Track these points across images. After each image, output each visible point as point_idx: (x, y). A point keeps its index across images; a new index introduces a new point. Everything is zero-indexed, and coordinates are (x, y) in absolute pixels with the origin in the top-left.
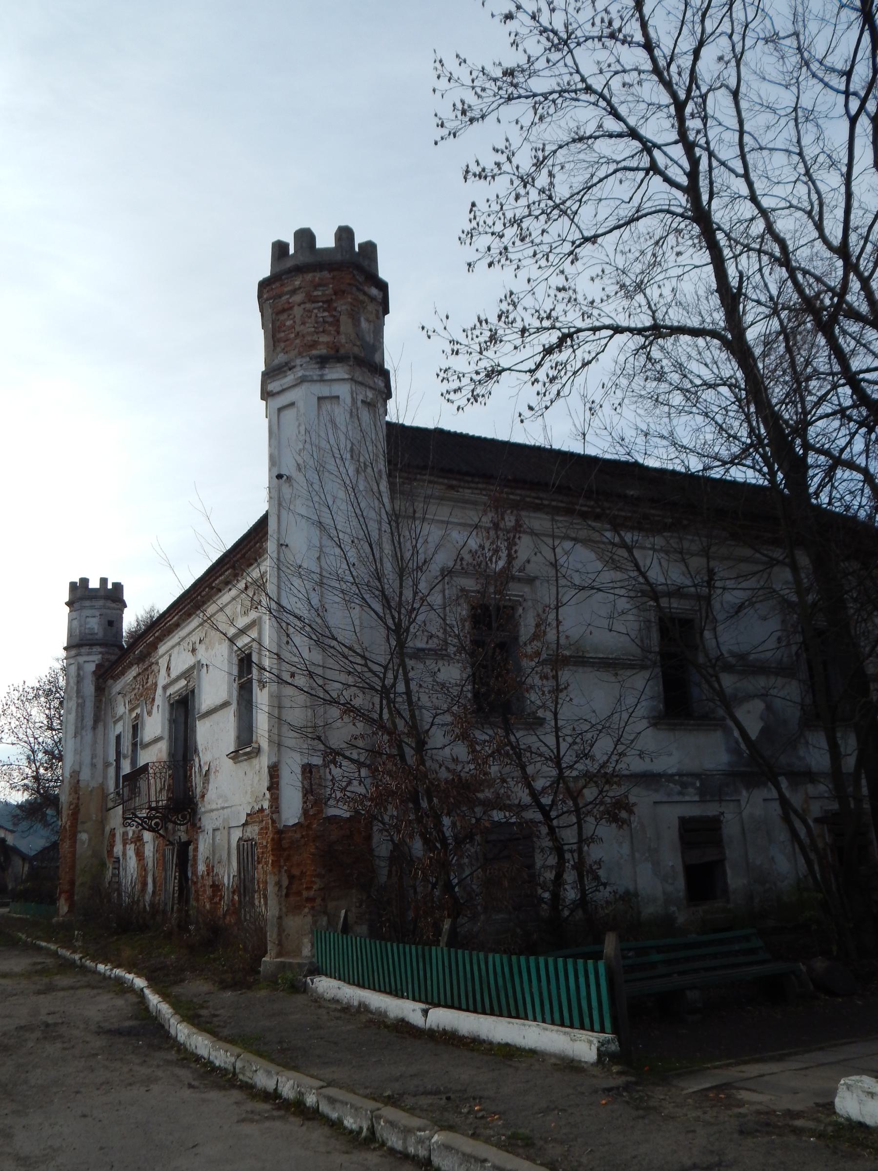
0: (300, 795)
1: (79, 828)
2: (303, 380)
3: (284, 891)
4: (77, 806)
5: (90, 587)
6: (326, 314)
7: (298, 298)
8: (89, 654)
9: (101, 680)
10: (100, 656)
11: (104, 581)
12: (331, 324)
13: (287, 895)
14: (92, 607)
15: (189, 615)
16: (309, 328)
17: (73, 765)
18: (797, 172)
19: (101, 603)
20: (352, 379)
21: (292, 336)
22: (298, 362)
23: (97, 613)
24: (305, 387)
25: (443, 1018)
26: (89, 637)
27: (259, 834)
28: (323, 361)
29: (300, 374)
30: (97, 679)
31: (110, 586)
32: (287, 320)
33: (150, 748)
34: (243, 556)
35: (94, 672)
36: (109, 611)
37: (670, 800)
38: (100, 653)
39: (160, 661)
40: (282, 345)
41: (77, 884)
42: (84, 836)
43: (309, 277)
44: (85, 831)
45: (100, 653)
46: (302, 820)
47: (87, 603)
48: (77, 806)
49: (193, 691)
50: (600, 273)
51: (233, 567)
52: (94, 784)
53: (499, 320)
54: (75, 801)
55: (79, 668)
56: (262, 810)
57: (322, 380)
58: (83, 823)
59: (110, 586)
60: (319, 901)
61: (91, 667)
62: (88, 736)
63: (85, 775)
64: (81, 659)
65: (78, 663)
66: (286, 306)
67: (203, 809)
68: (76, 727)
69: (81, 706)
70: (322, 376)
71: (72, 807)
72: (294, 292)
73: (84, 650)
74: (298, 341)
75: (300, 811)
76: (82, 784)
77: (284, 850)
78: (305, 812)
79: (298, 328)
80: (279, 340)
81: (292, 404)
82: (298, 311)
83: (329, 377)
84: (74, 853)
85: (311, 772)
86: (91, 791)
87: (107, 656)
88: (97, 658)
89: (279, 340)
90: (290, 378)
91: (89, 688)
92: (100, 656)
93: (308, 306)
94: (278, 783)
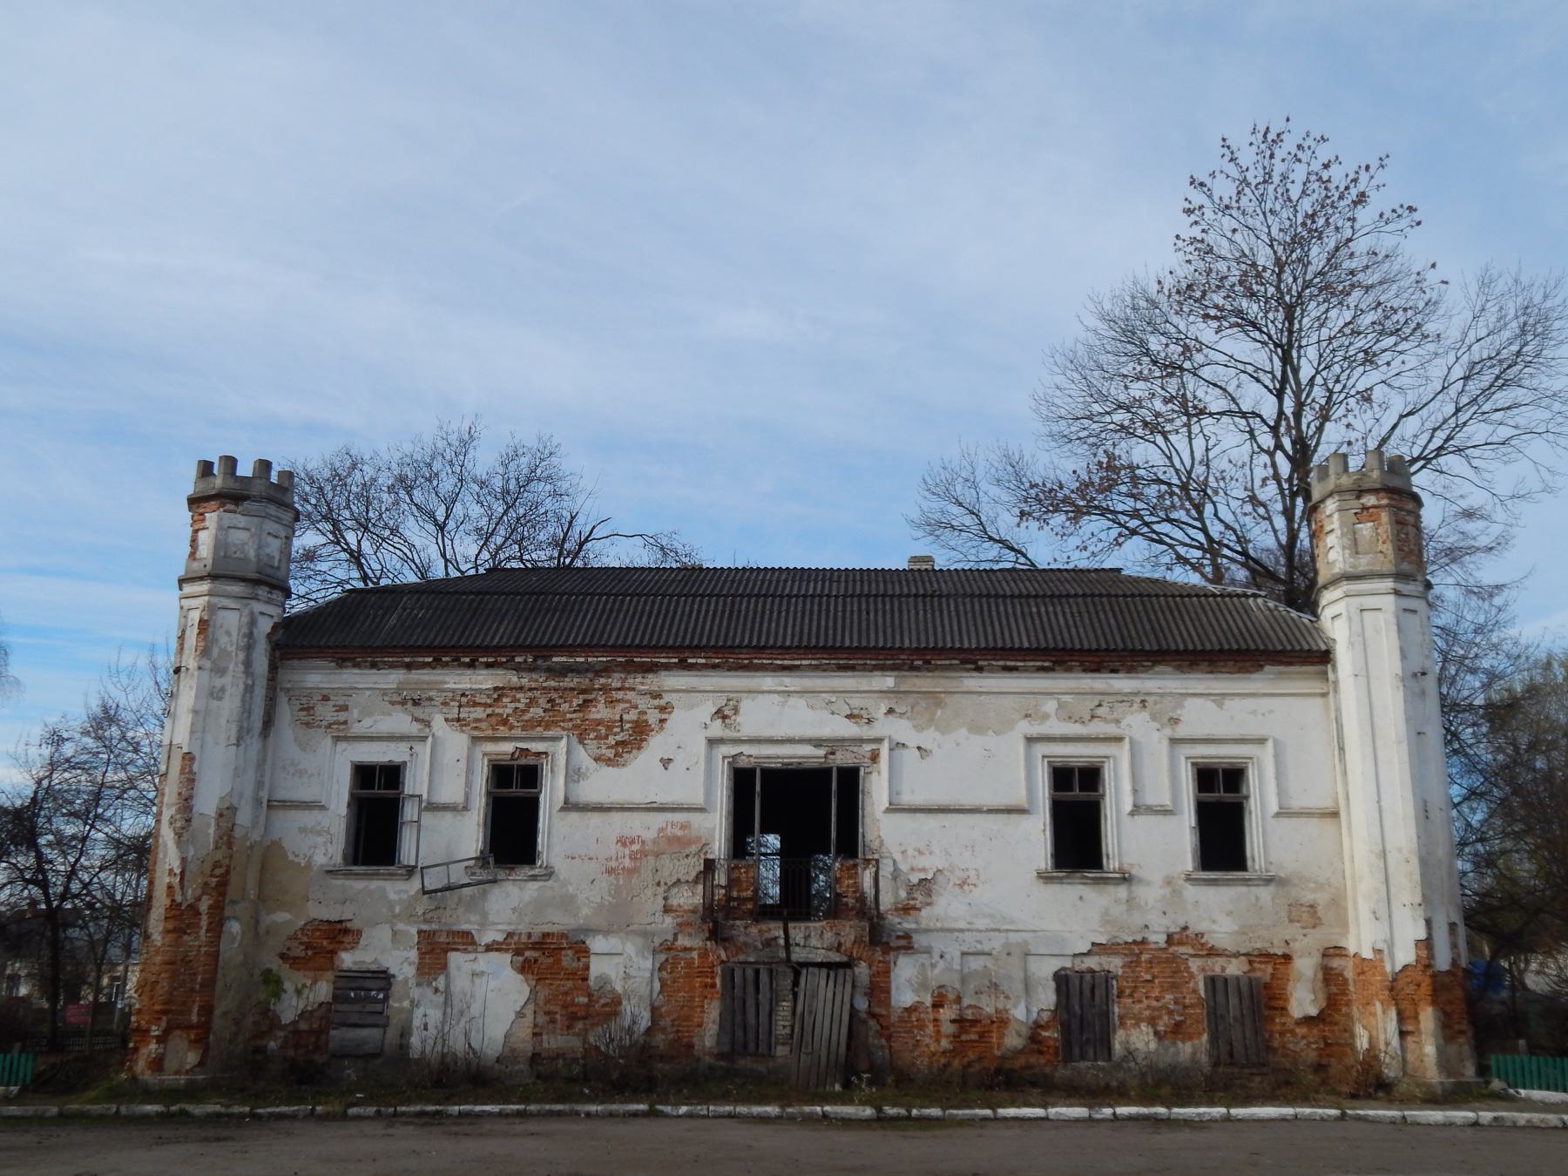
1: (228, 912)
5: (239, 473)
8: (269, 602)
9: (278, 654)
11: (265, 466)
15: (883, 668)
17: (230, 794)
25: (478, 1108)
30: (273, 650)
31: (274, 479)
33: (440, 814)
37: (680, 817)
41: (217, 1012)
42: (234, 927)
44: (235, 918)
50: (1374, 165)
52: (255, 836)
53: (1363, 194)
55: (253, 623)
56: (1144, 942)
58: (233, 902)
59: (274, 479)
62: (254, 743)
63: (244, 818)
64: (258, 607)
65: (252, 613)
68: (240, 729)
69: (249, 689)
71: (218, 871)
73: (262, 591)
76: (238, 833)
84: (216, 955)
86: (251, 847)
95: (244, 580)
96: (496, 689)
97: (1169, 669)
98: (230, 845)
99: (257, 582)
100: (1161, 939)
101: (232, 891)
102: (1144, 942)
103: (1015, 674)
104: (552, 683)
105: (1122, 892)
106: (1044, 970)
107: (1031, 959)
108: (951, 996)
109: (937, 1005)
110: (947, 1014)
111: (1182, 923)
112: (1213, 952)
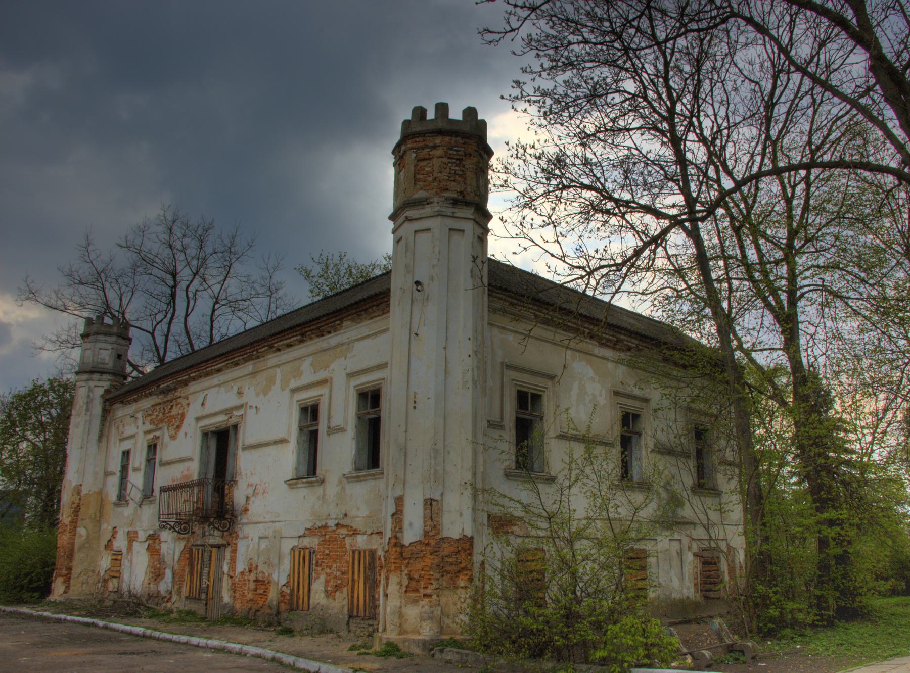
0: (422, 521)
1: (79, 523)
2: (440, 215)
3: (404, 589)
4: (78, 506)
6: (457, 168)
7: (439, 152)
8: (100, 380)
9: (108, 403)
10: (108, 383)
12: (460, 176)
13: (406, 591)
14: (106, 342)
16: (444, 176)
18: (495, 14)
19: (114, 339)
20: (474, 220)
21: (430, 179)
22: (436, 199)
23: (109, 346)
24: (439, 219)
26: (100, 366)
27: (319, 544)
28: (455, 202)
29: (437, 209)
30: (105, 402)
32: (426, 166)
34: (318, 328)
35: (102, 396)
36: (119, 347)
38: (109, 380)
39: (190, 397)
40: (421, 184)
43: (447, 139)
45: (109, 380)
46: (422, 538)
47: (101, 338)
48: (78, 506)
49: (236, 427)
51: (302, 335)
54: (77, 501)
56: (326, 527)
57: (453, 217)
60: (434, 597)
61: (101, 391)
64: (92, 384)
66: (427, 156)
67: (244, 521)
70: (454, 213)
72: (435, 147)
73: (96, 376)
74: (435, 184)
75: (422, 531)
77: (405, 559)
78: (426, 533)
79: (436, 175)
80: (419, 180)
81: (429, 230)
82: (436, 162)
83: (456, 215)
85: (431, 504)
87: (115, 383)
88: (106, 385)
89: (419, 180)
90: (428, 210)
91: (97, 408)
92: (108, 383)
93: (445, 160)
94: (402, 511)
95: (86, 372)
96: (153, 406)
97: (349, 323)
98: (79, 494)
99: (92, 372)
100: (332, 523)
101: (81, 514)
102: (326, 527)
103: (292, 348)
104: (165, 399)
105: (319, 490)
106: (287, 546)
107: (283, 540)
108: (254, 565)
109: (250, 571)
110: (252, 577)
111: (344, 512)
112: (355, 533)
